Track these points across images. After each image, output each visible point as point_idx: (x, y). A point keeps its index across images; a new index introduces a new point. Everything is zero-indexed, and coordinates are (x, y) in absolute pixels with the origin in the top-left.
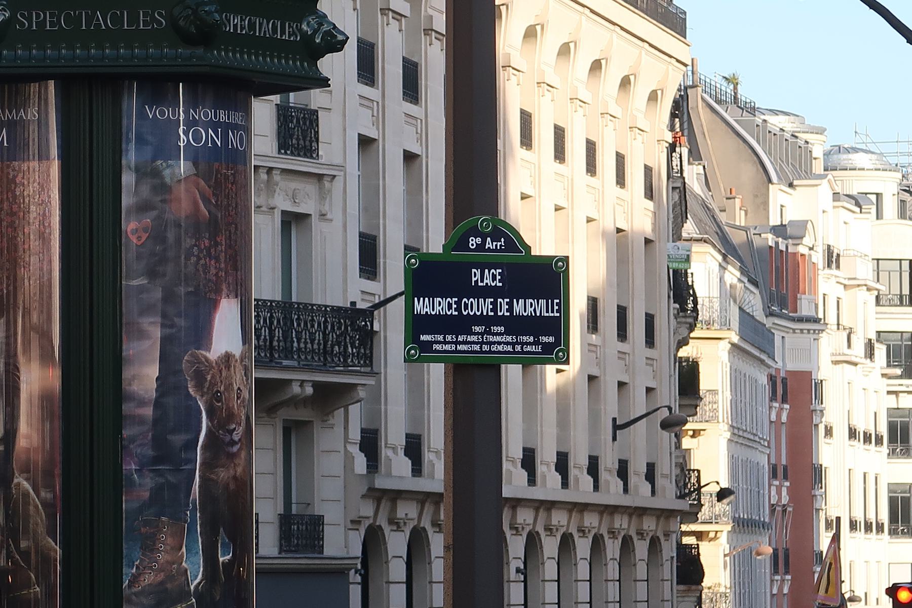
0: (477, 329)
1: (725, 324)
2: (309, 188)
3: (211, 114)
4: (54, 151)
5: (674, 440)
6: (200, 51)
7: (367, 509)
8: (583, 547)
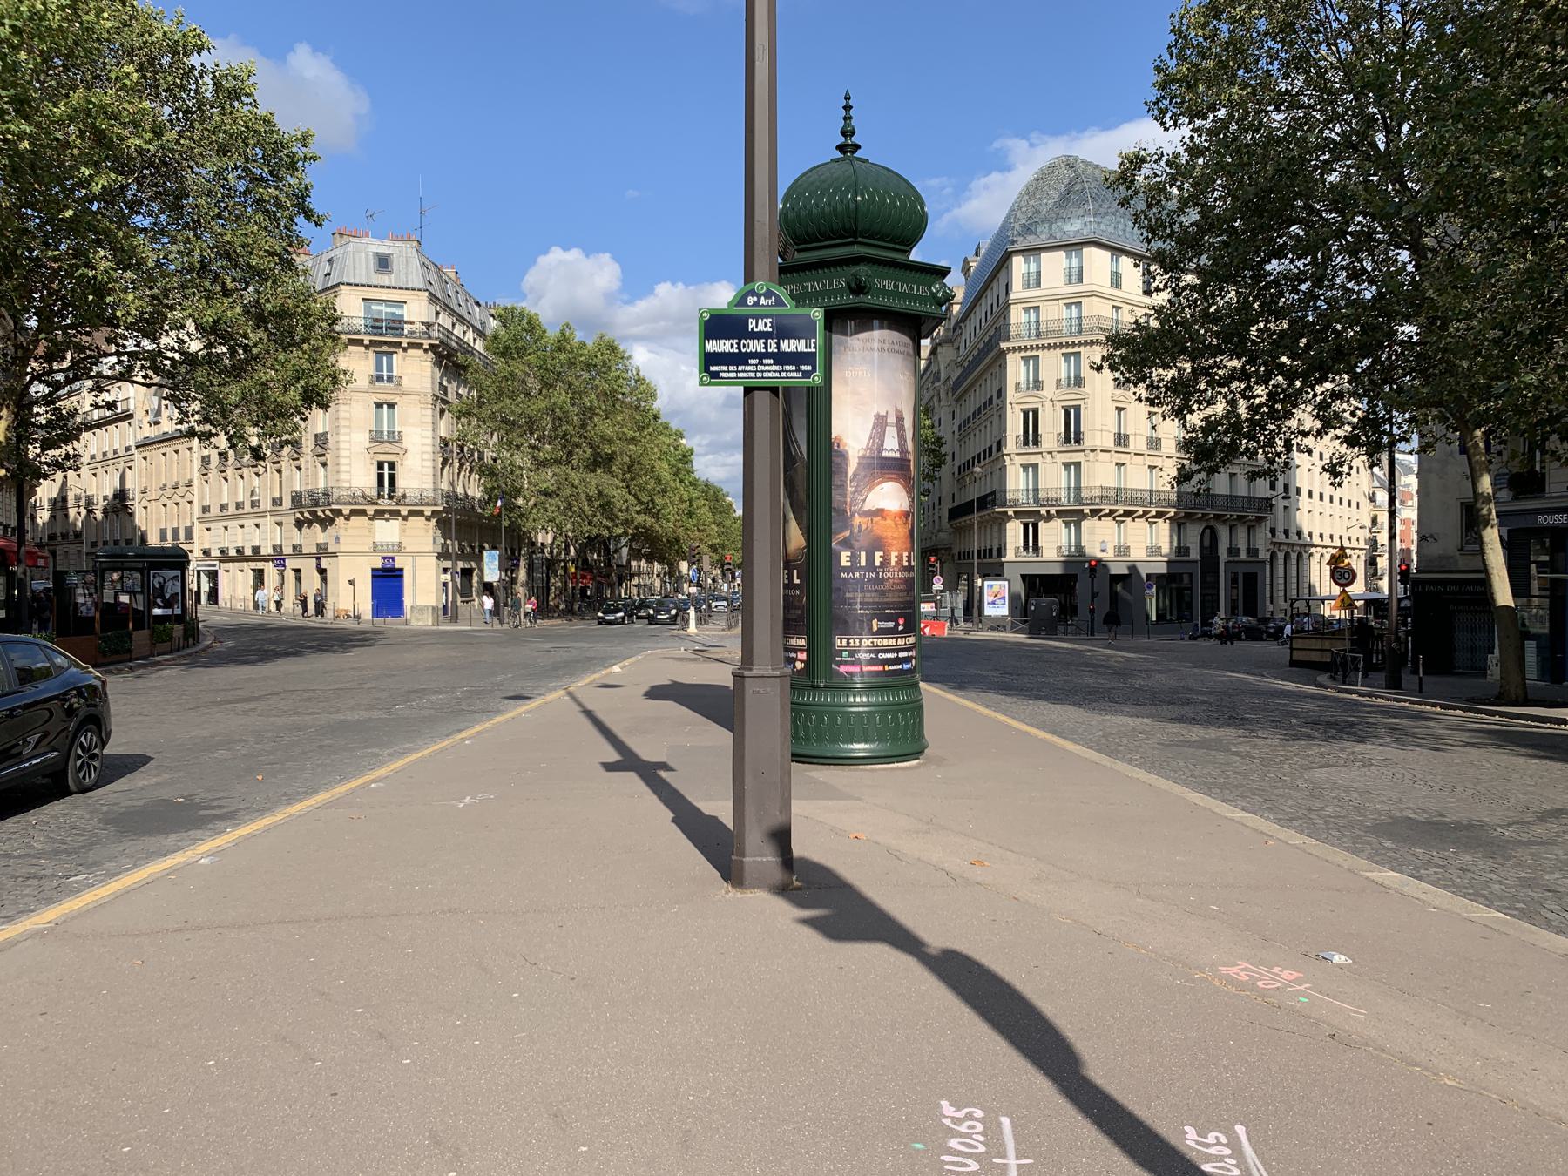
0: (752, 361)
7: (1272, 547)
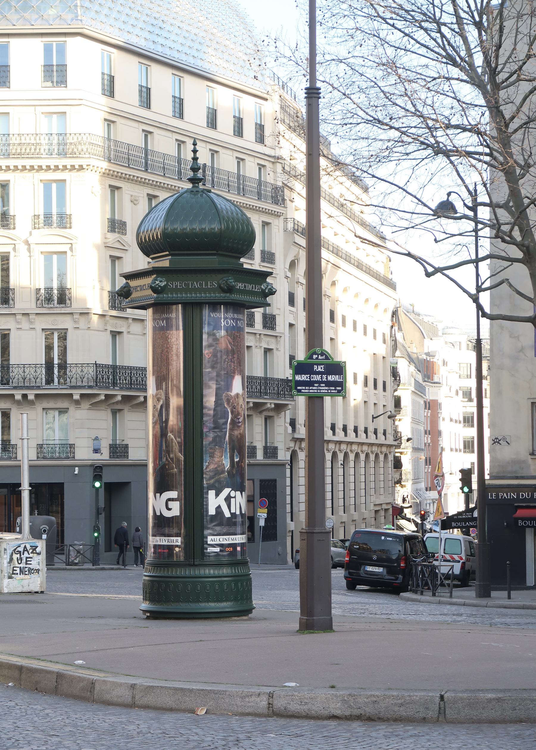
0: (316, 385)
1: (410, 384)
2: (273, 340)
3: (232, 315)
4: (181, 327)
5: (393, 422)
6: (228, 295)
7: (292, 444)
8: (362, 457)
